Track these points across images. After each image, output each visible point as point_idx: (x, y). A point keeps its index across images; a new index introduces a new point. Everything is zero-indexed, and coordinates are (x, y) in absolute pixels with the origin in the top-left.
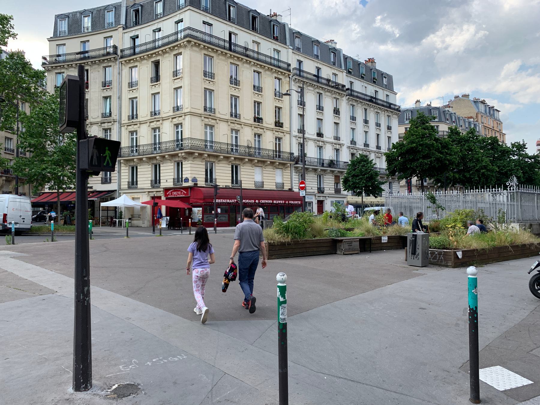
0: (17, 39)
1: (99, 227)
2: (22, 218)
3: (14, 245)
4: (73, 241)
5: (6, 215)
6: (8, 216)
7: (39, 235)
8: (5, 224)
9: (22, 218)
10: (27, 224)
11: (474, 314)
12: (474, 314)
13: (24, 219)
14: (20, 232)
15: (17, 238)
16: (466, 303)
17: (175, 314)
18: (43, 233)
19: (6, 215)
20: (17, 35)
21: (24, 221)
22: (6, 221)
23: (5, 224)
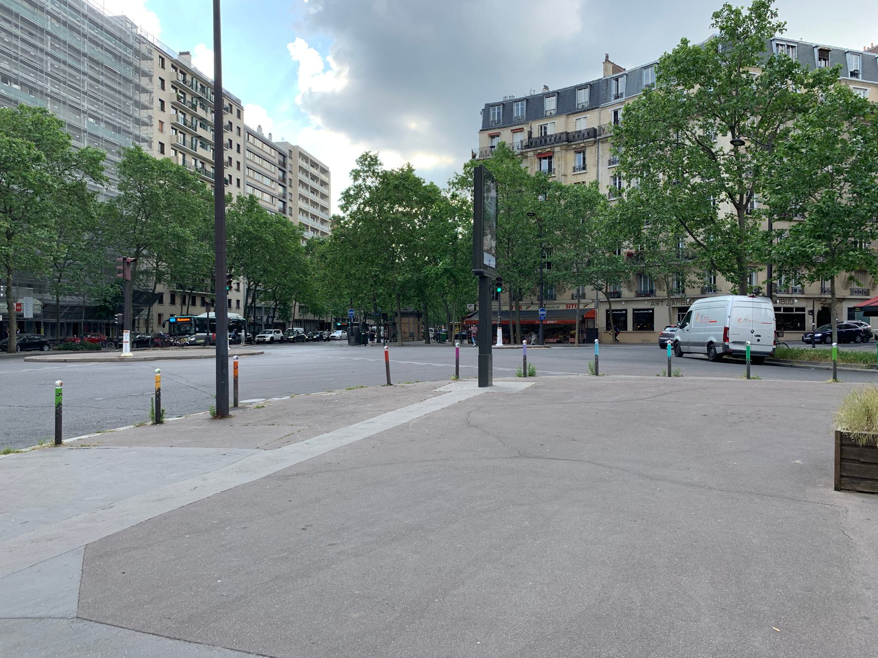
0: (786, 30)
1: (112, 355)
2: (754, 334)
3: (597, 377)
4: (500, 369)
5: (728, 329)
6: (730, 331)
7: (791, 366)
8: (726, 343)
9: (754, 334)
10: (767, 345)
11: (59, 407)
12: (59, 407)
13: (760, 336)
14: (759, 359)
15: (755, 370)
16: (52, 400)
17: (61, 412)
18: (801, 363)
19: (728, 329)
20: (786, 23)
21: (759, 340)
22: (728, 339)
23: (726, 343)
